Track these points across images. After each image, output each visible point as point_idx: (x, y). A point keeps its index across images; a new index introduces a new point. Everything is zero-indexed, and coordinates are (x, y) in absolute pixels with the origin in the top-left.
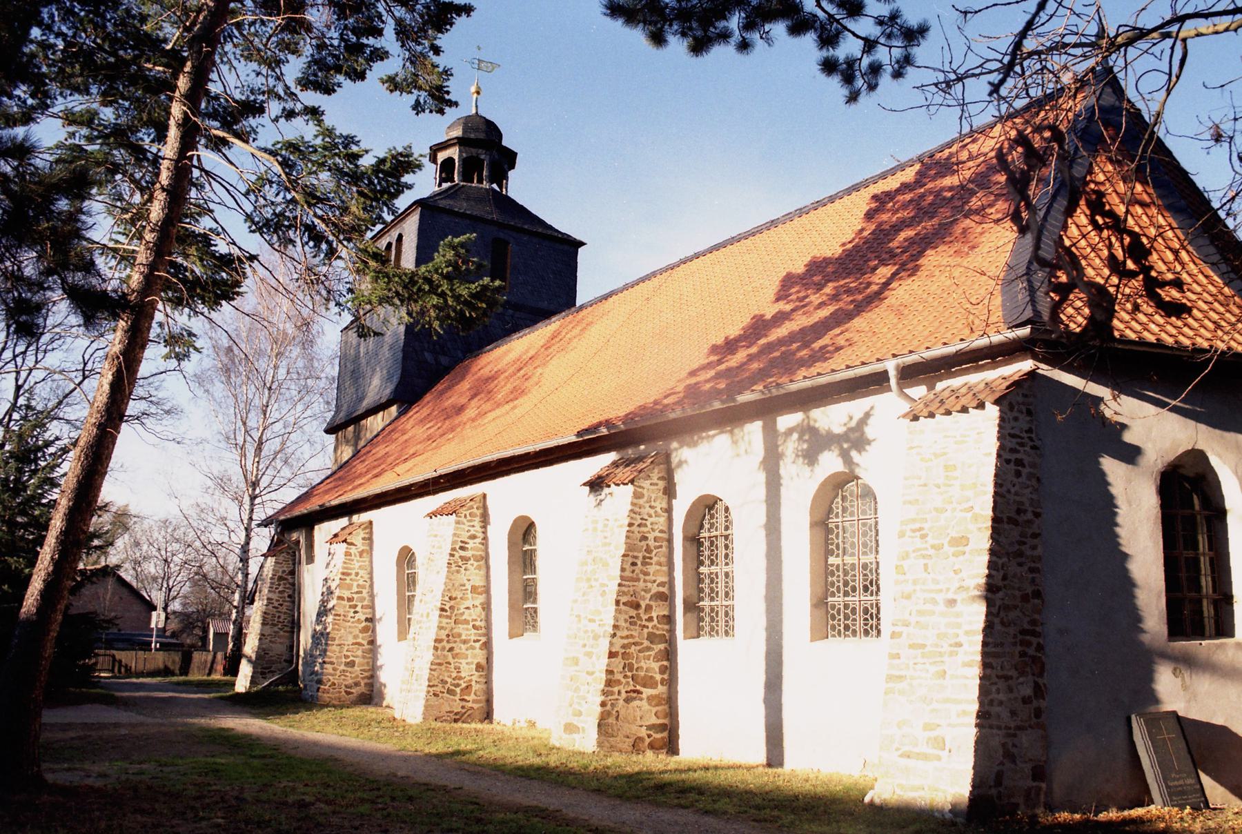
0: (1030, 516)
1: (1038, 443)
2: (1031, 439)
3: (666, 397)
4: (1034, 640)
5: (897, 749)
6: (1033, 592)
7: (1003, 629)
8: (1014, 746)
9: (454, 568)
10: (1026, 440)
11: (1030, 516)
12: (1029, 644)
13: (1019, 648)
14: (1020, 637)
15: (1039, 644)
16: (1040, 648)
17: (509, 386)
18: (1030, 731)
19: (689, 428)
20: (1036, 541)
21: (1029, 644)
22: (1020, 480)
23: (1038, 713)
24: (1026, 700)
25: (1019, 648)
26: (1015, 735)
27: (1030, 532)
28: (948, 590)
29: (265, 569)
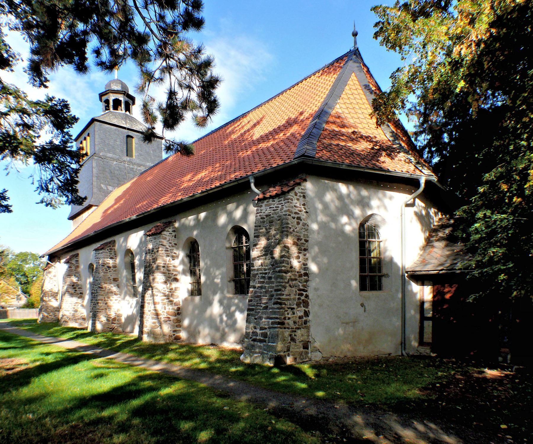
0: (303, 241)
1: (308, 210)
2: (305, 209)
3: (138, 202)
4: (305, 293)
5: (251, 338)
6: (304, 273)
7: (290, 288)
8: (295, 335)
9: (77, 275)
10: (303, 209)
11: (303, 241)
12: (302, 295)
13: (297, 297)
14: (298, 292)
15: (306, 294)
16: (307, 296)
17: (126, 363)
18: (302, 329)
19: (351, 198)
20: (306, 253)
21: (302, 295)
22: (299, 226)
23: (306, 322)
24: (300, 317)
25: (297, 297)
26: (295, 331)
27: (303, 248)
28: (269, 273)
29: (245, 120)
